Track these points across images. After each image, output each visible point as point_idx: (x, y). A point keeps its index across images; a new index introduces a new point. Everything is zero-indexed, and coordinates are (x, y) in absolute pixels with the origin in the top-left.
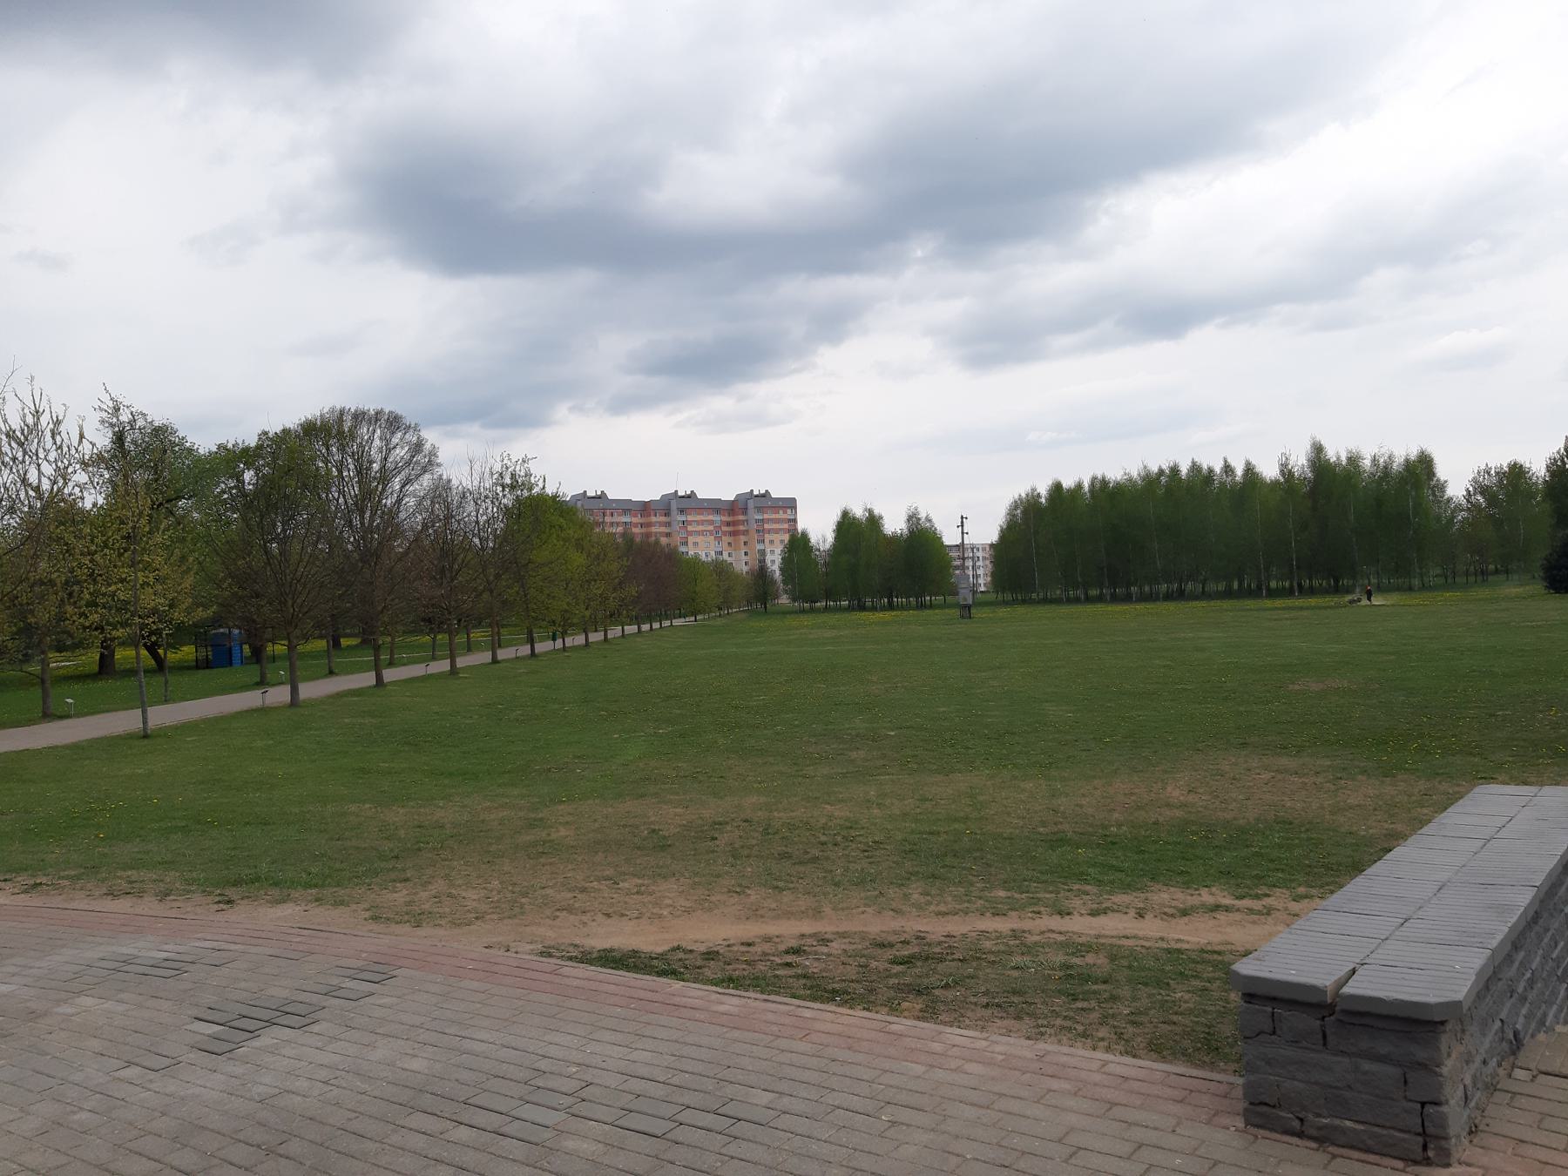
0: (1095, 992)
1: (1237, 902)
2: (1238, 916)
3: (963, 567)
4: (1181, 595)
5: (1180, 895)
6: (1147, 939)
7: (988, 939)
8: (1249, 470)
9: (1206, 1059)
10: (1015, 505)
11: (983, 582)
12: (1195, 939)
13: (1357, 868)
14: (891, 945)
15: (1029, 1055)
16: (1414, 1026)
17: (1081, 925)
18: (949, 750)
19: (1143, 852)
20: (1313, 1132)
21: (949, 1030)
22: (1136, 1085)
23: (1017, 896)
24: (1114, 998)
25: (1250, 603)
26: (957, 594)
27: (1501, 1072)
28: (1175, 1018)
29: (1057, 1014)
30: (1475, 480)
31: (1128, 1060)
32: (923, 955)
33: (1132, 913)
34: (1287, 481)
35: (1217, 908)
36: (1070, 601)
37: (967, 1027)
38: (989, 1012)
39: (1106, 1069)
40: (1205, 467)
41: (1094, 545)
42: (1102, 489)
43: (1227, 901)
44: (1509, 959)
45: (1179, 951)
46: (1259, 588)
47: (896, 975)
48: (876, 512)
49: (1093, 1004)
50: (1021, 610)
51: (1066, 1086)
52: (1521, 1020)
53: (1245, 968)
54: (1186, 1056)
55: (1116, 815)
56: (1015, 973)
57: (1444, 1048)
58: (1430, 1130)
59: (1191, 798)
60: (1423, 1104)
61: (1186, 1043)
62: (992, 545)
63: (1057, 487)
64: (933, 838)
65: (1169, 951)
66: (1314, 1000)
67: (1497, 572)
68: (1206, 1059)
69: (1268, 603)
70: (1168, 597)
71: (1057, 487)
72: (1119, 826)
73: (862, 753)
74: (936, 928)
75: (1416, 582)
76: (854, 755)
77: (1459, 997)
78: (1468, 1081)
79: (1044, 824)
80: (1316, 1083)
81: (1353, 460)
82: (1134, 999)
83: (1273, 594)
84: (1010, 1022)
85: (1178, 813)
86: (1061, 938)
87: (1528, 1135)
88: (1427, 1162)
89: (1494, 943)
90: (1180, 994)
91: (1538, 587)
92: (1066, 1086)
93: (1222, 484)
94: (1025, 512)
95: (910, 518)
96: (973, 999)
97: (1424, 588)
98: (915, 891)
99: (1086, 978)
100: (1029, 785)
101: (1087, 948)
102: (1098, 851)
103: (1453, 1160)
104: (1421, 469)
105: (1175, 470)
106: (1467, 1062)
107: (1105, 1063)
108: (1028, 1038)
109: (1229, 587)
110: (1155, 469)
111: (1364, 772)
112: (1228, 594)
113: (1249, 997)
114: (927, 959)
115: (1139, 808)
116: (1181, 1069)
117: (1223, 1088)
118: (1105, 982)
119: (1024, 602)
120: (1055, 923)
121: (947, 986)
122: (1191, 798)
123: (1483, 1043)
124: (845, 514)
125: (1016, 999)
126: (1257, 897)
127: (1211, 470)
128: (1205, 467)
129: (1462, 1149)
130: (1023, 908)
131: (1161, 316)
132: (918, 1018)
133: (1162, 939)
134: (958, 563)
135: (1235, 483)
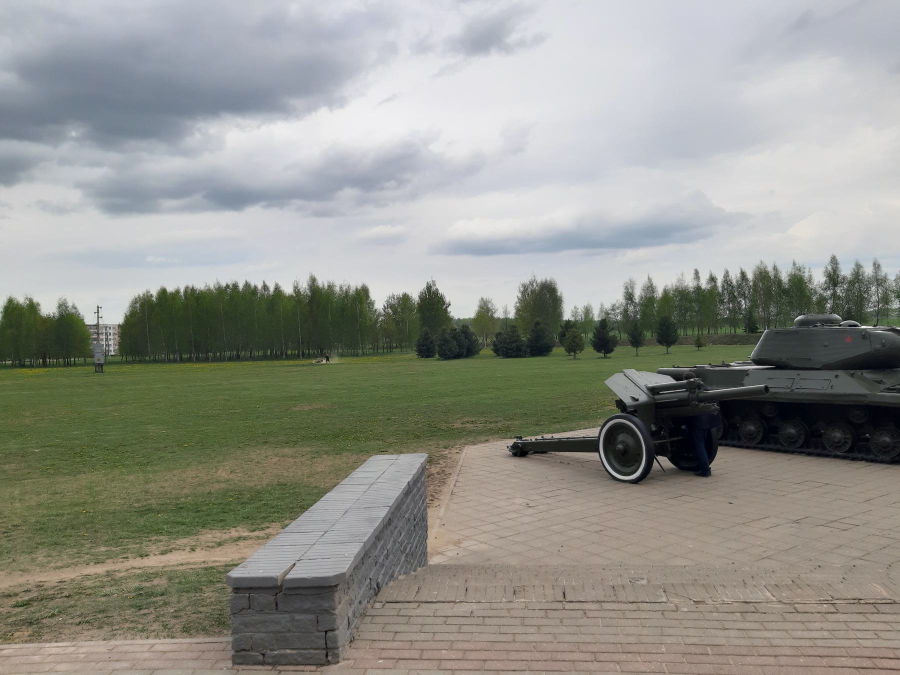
0: (154, 603)
1: (251, 534)
2: (250, 542)
3: (97, 339)
4: (238, 358)
5: (218, 535)
6: (194, 563)
7: (89, 579)
8: (277, 288)
9: (217, 630)
10: (135, 302)
11: (113, 349)
12: (224, 559)
13: (304, 508)
14: (16, 595)
15: (102, 649)
16: (322, 589)
17: (154, 562)
18: (78, 460)
19: (199, 511)
20: (270, 660)
21: (48, 645)
22: (170, 655)
23: (114, 549)
24: (166, 604)
25: (276, 363)
26: (93, 357)
27: (369, 606)
28: (201, 609)
29: (127, 620)
30: (388, 301)
31: (168, 640)
32: (43, 596)
33: (188, 549)
34: (297, 296)
35: (239, 539)
36: (170, 361)
37: (63, 641)
38: (80, 627)
39: (153, 649)
40: (253, 285)
41: (175, 327)
42: (192, 295)
43: (246, 534)
44: (374, 545)
45: (212, 568)
46: (282, 354)
47: (15, 615)
48: (35, 300)
49: (152, 609)
50: (138, 367)
51: (125, 665)
52: (381, 576)
53: (235, 573)
54: (205, 631)
55: (185, 491)
56: (104, 599)
57: (337, 599)
58: (330, 645)
59: (231, 476)
60: (326, 632)
61: (206, 623)
62: (119, 326)
63: (163, 292)
64: (58, 519)
65: (206, 569)
66: (270, 585)
67: (397, 347)
68: (217, 630)
69: (286, 363)
70: (230, 359)
71: (163, 292)
72: (187, 496)
73: (13, 466)
74: (51, 578)
75: (360, 351)
76: (7, 467)
77: (345, 570)
78: (350, 614)
79: (138, 501)
80: (272, 632)
81: (331, 287)
82: (179, 602)
83: (288, 358)
84: (95, 632)
85: (223, 485)
86: (139, 572)
87: (376, 636)
88: (328, 663)
89: (366, 539)
90: (209, 594)
91: (413, 355)
92: (125, 665)
93: (263, 295)
94: (142, 305)
95: (60, 306)
96: (70, 621)
97: (364, 355)
98: (40, 555)
99: (151, 595)
100: (131, 478)
101: (157, 575)
102: (171, 514)
103: (340, 659)
104: (363, 294)
105: (235, 286)
106: (350, 605)
107: (153, 645)
108: (105, 640)
109: (265, 353)
110: (224, 285)
111: (327, 453)
112: (265, 358)
113: (237, 590)
114: (42, 600)
115: (200, 485)
116: (200, 639)
117: (223, 646)
118: (162, 595)
119: (140, 362)
120: (138, 562)
121: (53, 616)
122: (231, 476)
123: (359, 592)
124: (10, 301)
125: (100, 616)
126: (263, 529)
127: (256, 287)
128: (253, 285)
129: (345, 651)
130: (117, 555)
131: (230, 196)
132: (26, 642)
133: (204, 562)
134: (95, 336)
135: (269, 296)
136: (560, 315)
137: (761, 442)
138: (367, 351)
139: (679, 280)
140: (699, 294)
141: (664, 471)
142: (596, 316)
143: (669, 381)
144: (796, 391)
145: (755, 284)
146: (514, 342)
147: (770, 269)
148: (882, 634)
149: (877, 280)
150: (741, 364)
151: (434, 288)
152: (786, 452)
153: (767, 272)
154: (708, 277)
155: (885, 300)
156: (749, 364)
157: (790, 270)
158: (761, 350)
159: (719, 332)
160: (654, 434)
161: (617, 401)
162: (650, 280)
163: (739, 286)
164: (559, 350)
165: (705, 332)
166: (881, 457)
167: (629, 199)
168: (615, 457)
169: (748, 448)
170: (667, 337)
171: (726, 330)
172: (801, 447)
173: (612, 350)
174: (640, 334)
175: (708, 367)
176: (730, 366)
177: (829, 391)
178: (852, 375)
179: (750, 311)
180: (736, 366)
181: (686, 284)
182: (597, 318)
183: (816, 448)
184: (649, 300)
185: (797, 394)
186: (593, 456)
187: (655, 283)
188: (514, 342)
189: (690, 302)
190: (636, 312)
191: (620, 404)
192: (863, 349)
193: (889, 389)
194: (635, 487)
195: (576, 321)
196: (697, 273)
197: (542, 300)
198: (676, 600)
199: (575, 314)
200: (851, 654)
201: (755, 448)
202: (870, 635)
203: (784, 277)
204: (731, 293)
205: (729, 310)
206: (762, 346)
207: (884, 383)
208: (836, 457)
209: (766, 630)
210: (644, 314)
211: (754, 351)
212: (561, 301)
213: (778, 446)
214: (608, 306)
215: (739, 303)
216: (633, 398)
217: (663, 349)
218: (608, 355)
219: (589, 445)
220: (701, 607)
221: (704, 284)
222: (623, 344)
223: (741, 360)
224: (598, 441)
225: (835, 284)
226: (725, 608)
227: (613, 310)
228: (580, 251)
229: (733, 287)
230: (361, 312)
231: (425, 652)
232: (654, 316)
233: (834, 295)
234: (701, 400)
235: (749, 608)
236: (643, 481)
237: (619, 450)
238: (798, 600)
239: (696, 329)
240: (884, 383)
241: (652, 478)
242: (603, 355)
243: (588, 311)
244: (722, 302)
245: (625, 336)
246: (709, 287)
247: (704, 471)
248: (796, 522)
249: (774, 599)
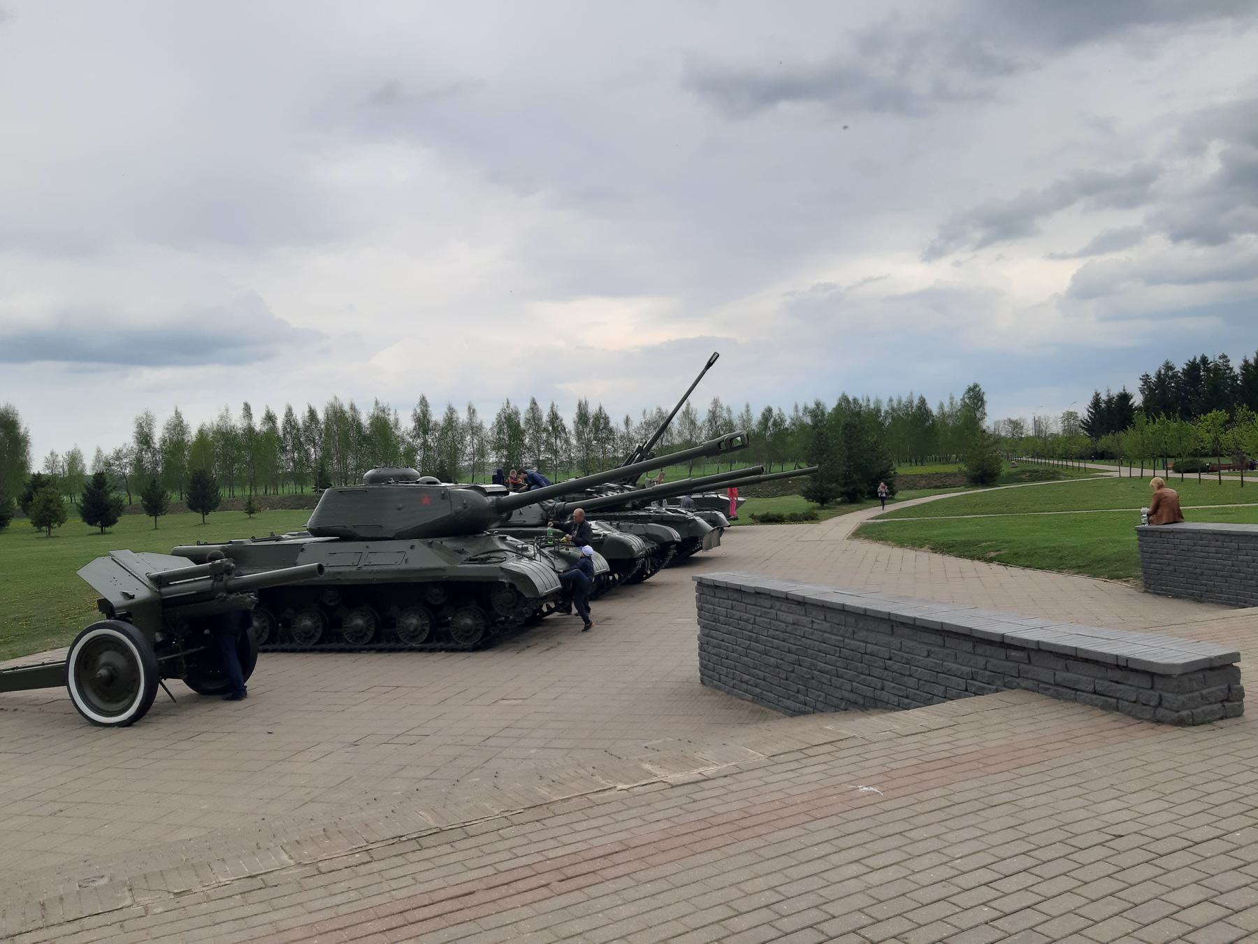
136: (24, 465)
137: (321, 641)
139: (222, 417)
140: (250, 439)
141: (176, 703)
142: (89, 467)
143: (186, 565)
144: (364, 568)
145: (327, 424)
147: (346, 408)
148: (420, 877)
149: (472, 428)
150: (292, 536)
151: (592, 410)
152: (351, 651)
153: (343, 412)
154: (263, 415)
155: (481, 452)
156: (304, 535)
157: (372, 411)
158: (319, 516)
159: (280, 491)
160: (158, 648)
161: (100, 602)
162: (178, 415)
163: (307, 428)
164: (21, 524)
165: (261, 492)
166: (463, 644)
167: (146, 292)
168: (95, 691)
169: (303, 651)
170: (203, 498)
171: (289, 489)
172: (371, 642)
173: (114, 522)
174: (161, 496)
175: (248, 542)
176: (281, 539)
177: (404, 566)
178: (430, 545)
179: (322, 463)
180: (288, 539)
181: (233, 423)
182: (89, 472)
183: (388, 641)
184: (175, 444)
185: (364, 572)
186: (59, 692)
187: (187, 419)
189: (239, 450)
190: (156, 463)
191: (105, 605)
192: (441, 512)
193: (471, 560)
194: (128, 732)
195: (55, 477)
196: (247, 408)
198: (145, 899)
199: (51, 462)
200: (381, 915)
201: (311, 651)
202: (409, 881)
203: (365, 420)
204: (296, 437)
205: (294, 461)
206: (322, 510)
207: (466, 553)
208: (412, 650)
209: (275, 910)
210: (168, 465)
211: (310, 518)
212: (27, 442)
213: (342, 645)
214: (109, 452)
215: (307, 452)
216: (126, 595)
217: (196, 517)
218: (108, 529)
219: (51, 676)
220: (185, 900)
221: (258, 424)
222: (134, 511)
223: (293, 529)
224: (67, 667)
225: (426, 432)
226: (222, 892)
227: (118, 458)
228: (63, 365)
229: (298, 430)
232: (183, 467)
233: (425, 443)
234: (230, 591)
235: (257, 882)
236: (144, 719)
237: (101, 677)
238: (324, 856)
239: (248, 488)
240: (466, 553)
241: (158, 714)
242: (99, 530)
243: (74, 459)
244: (284, 450)
245: (137, 499)
246: (265, 429)
247: (235, 691)
248: (355, 744)
249: (292, 862)
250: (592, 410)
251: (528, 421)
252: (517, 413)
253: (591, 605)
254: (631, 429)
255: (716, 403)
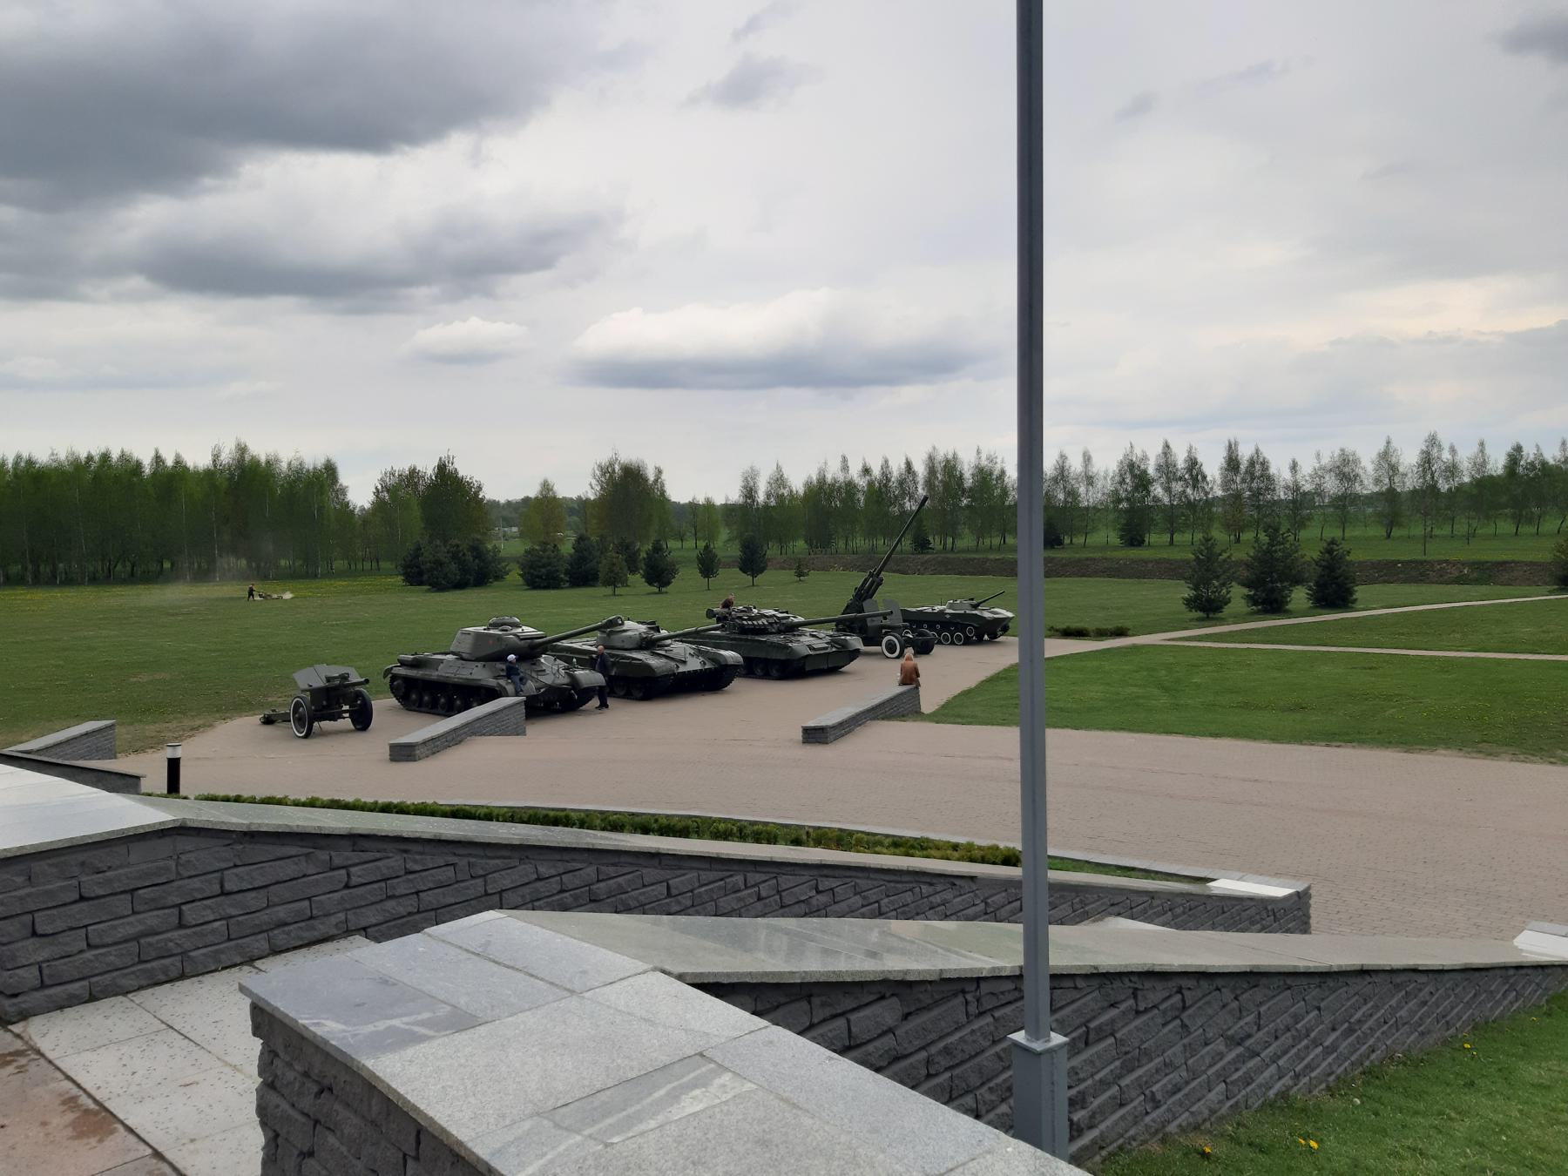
105: (105, 457)
138: (339, 564)
146: (544, 566)
154: (860, 467)
173: (669, 583)
187: (787, 473)
188: (544, 566)
196: (845, 460)
197: (629, 490)
221: (855, 472)
230: (320, 509)
231: (216, 889)
250: (1245, 453)
251: (1159, 468)
252: (1145, 458)
253: (1055, 931)
254: (1299, 477)
255: (1433, 441)
